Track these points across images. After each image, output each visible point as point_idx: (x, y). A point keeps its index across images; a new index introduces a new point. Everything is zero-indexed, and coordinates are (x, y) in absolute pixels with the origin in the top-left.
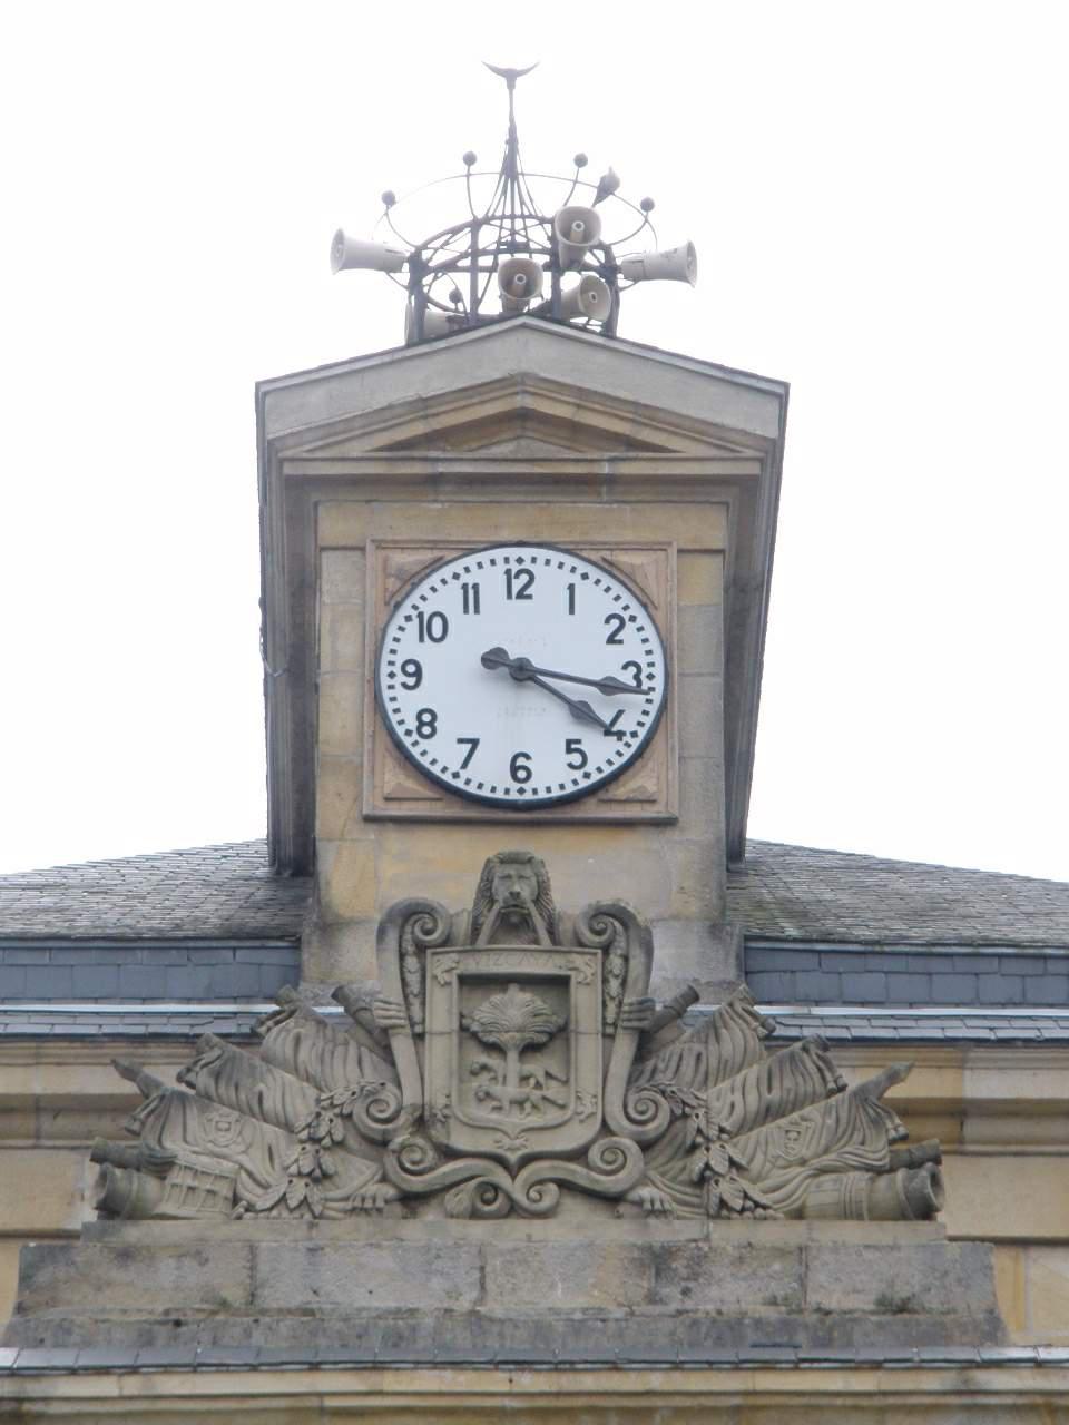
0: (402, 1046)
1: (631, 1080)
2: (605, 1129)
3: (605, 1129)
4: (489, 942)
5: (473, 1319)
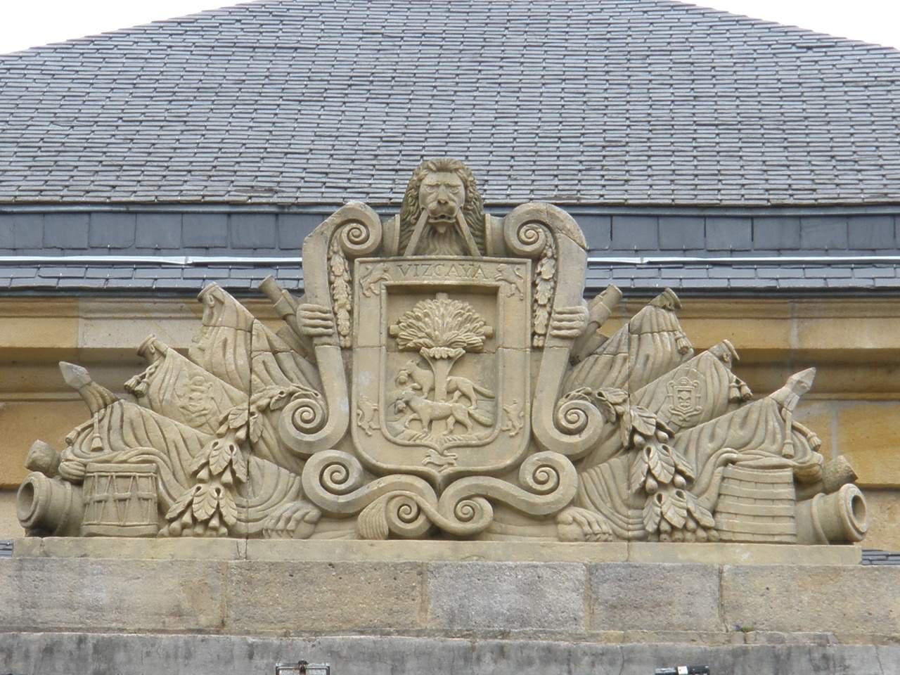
0: (330, 358)
1: (563, 393)
2: (535, 444)
3: (535, 444)
4: (415, 254)
5: (398, 657)
